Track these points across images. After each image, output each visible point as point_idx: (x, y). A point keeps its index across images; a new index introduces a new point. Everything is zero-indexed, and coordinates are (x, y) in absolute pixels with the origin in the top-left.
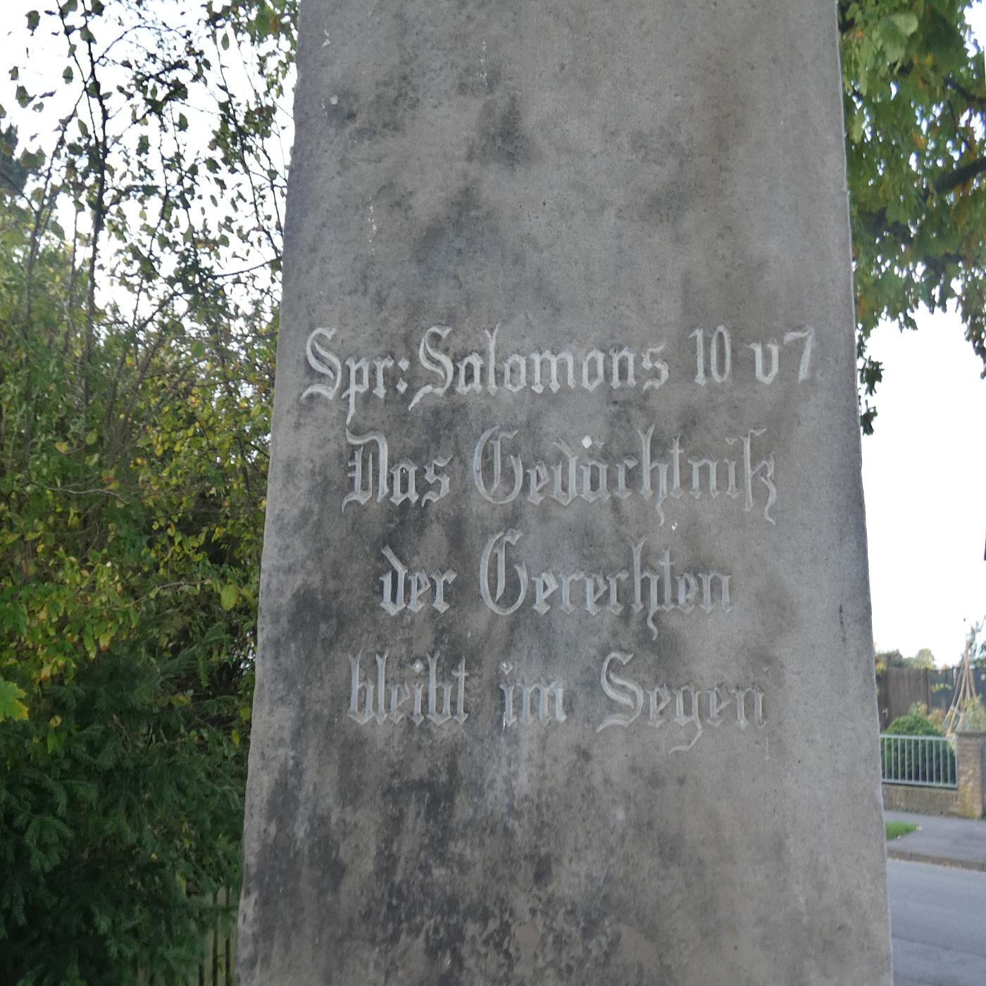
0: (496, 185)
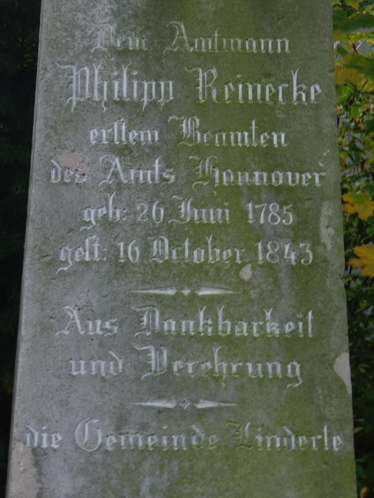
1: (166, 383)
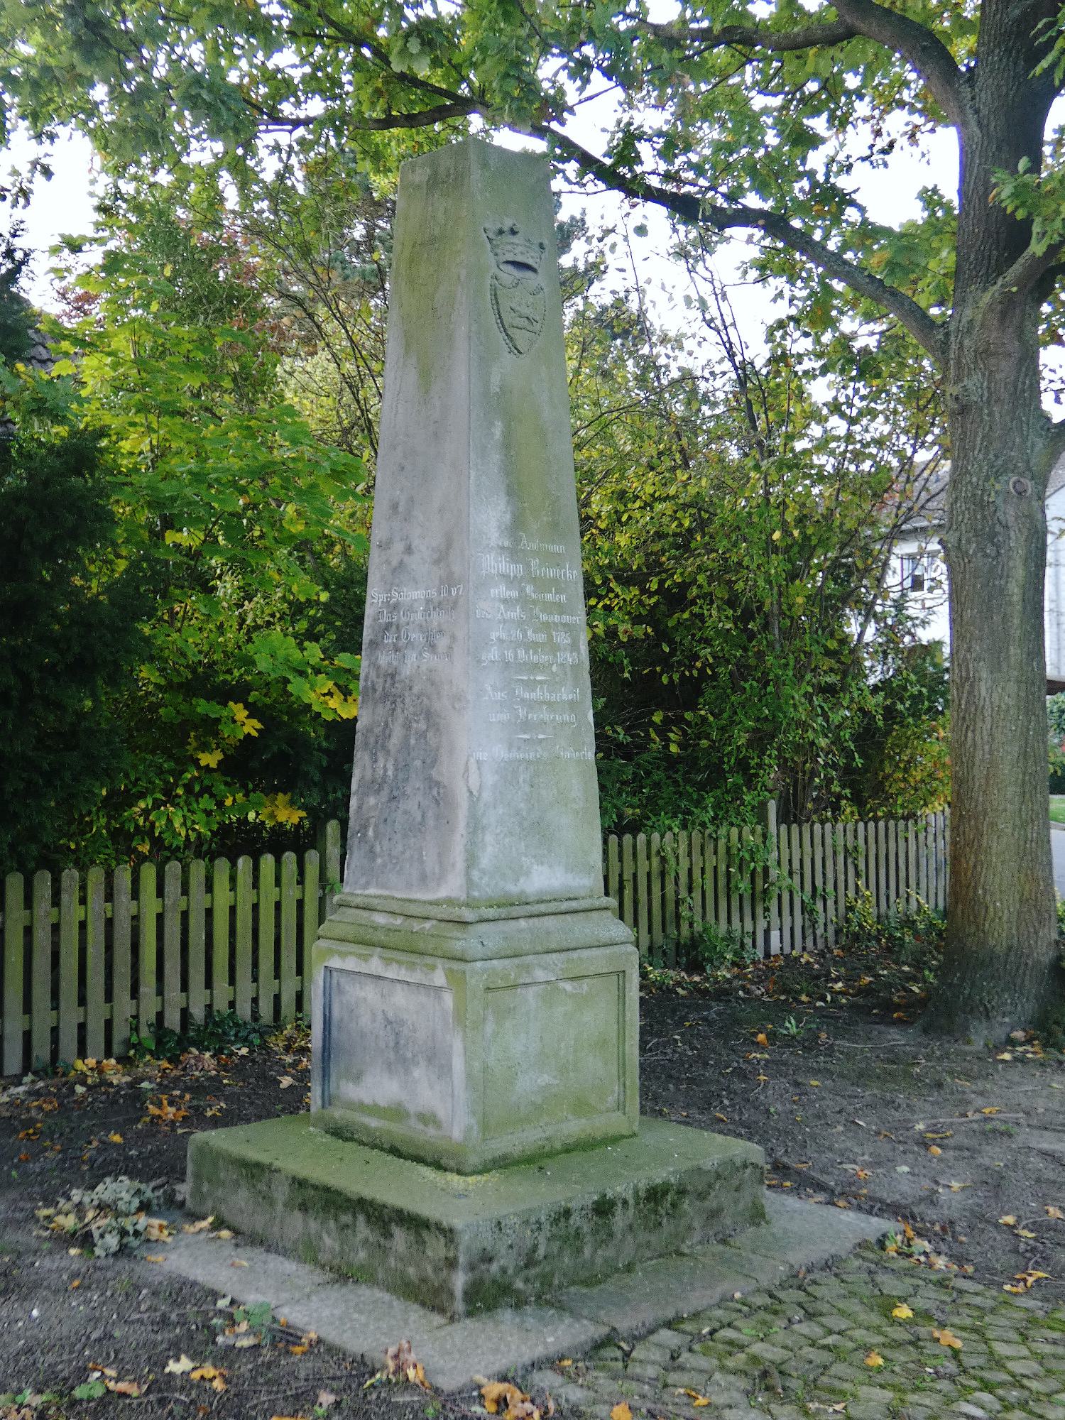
0: (406, 559)
1: (526, 725)
